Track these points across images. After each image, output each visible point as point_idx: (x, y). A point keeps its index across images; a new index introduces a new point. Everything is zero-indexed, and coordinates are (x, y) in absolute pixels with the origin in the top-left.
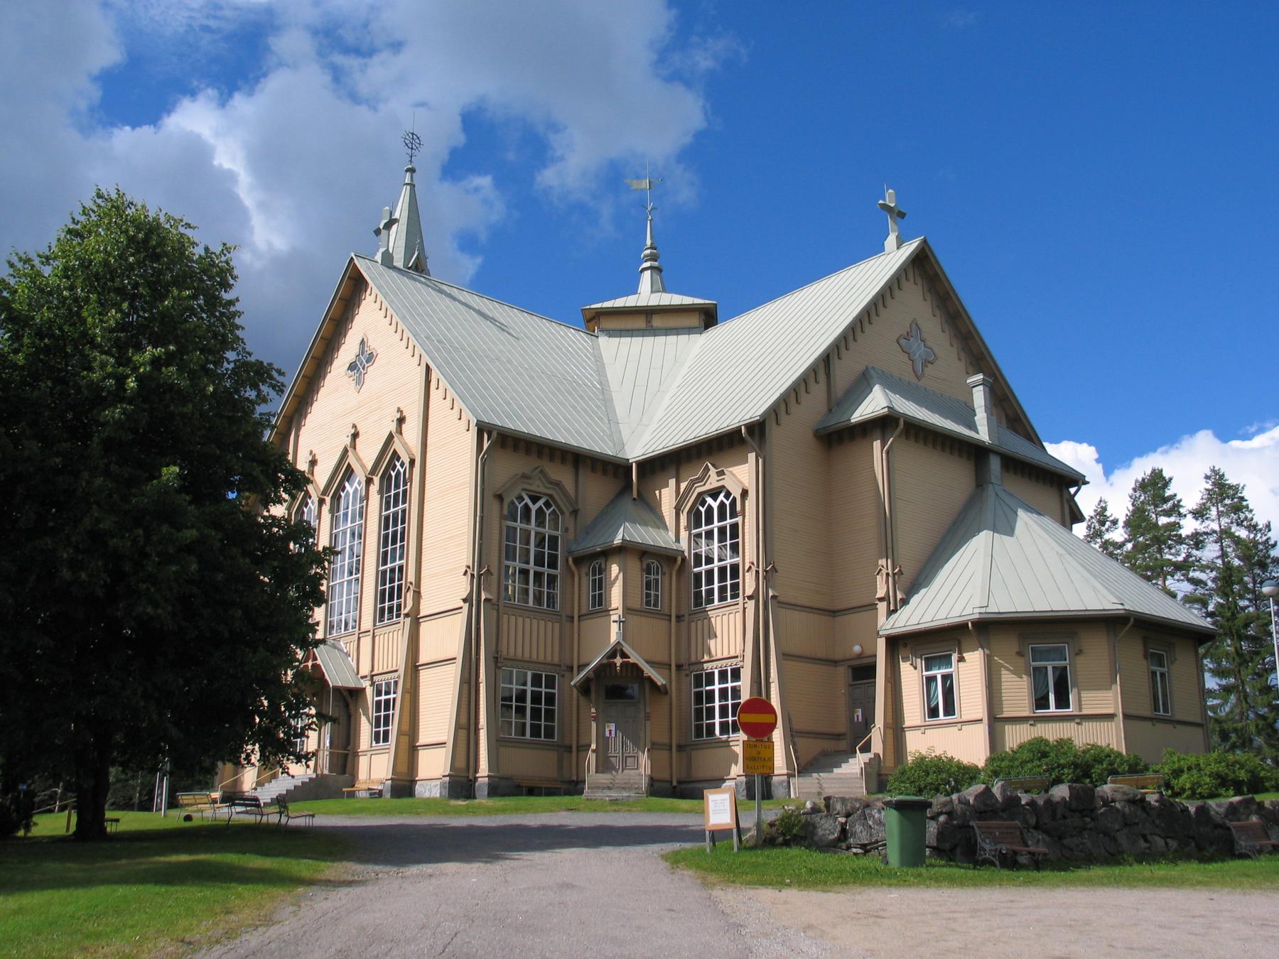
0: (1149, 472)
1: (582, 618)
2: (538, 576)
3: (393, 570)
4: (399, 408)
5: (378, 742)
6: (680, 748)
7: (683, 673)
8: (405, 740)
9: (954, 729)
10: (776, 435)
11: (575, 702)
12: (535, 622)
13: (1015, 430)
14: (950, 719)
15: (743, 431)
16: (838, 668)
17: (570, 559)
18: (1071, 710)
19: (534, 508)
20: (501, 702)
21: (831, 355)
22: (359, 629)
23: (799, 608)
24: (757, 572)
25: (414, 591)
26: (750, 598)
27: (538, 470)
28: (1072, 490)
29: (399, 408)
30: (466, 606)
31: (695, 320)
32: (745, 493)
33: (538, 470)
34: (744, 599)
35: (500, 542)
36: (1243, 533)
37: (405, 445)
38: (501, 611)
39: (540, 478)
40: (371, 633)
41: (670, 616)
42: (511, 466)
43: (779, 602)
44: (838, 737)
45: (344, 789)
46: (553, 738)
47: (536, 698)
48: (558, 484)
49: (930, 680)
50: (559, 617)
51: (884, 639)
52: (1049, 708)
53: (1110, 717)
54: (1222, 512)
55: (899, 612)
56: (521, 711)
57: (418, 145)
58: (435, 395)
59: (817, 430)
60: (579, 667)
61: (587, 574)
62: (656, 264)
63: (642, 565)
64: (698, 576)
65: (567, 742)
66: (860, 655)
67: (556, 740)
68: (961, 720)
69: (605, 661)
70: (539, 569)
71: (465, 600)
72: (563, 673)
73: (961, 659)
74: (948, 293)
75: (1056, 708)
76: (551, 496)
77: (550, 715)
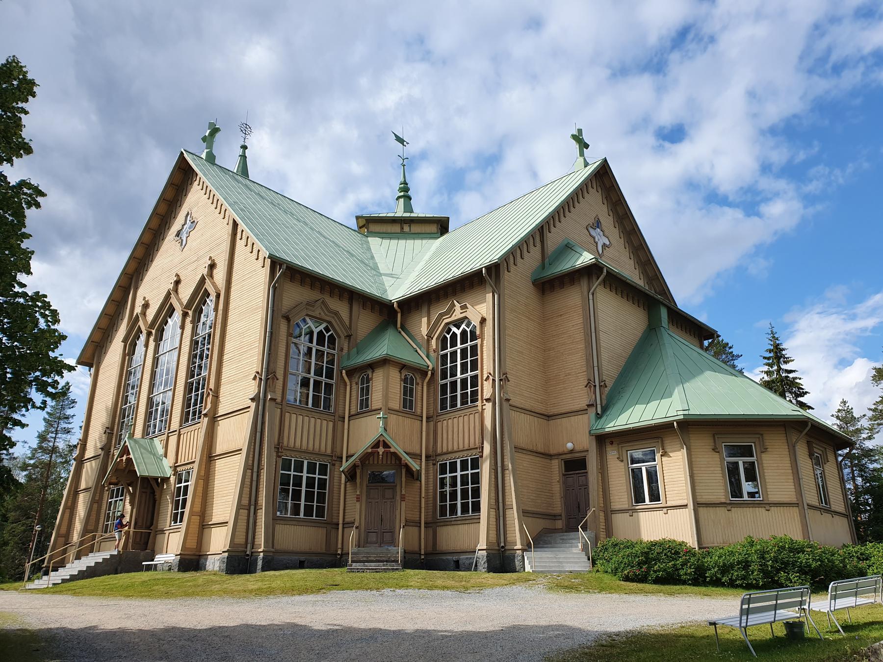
1: (352, 418)
2: (317, 384)
7: (431, 462)
8: (196, 519)
9: (660, 513)
10: (507, 277)
11: (343, 486)
14: (655, 504)
15: (484, 272)
16: (553, 461)
17: (344, 372)
22: (169, 430)
24: (494, 380)
25: (213, 396)
26: (488, 400)
30: (253, 405)
31: (434, 228)
32: (483, 321)
37: (214, 284)
41: (422, 417)
44: (554, 517)
45: (143, 563)
47: (310, 483)
48: (336, 314)
50: (333, 418)
53: (686, 506)
56: (297, 495)
60: (347, 457)
63: (401, 376)
65: (335, 521)
66: (571, 450)
67: (325, 519)
68: (667, 505)
71: (252, 400)
72: (334, 462)
73: (665, 454)
77: (321, 498)
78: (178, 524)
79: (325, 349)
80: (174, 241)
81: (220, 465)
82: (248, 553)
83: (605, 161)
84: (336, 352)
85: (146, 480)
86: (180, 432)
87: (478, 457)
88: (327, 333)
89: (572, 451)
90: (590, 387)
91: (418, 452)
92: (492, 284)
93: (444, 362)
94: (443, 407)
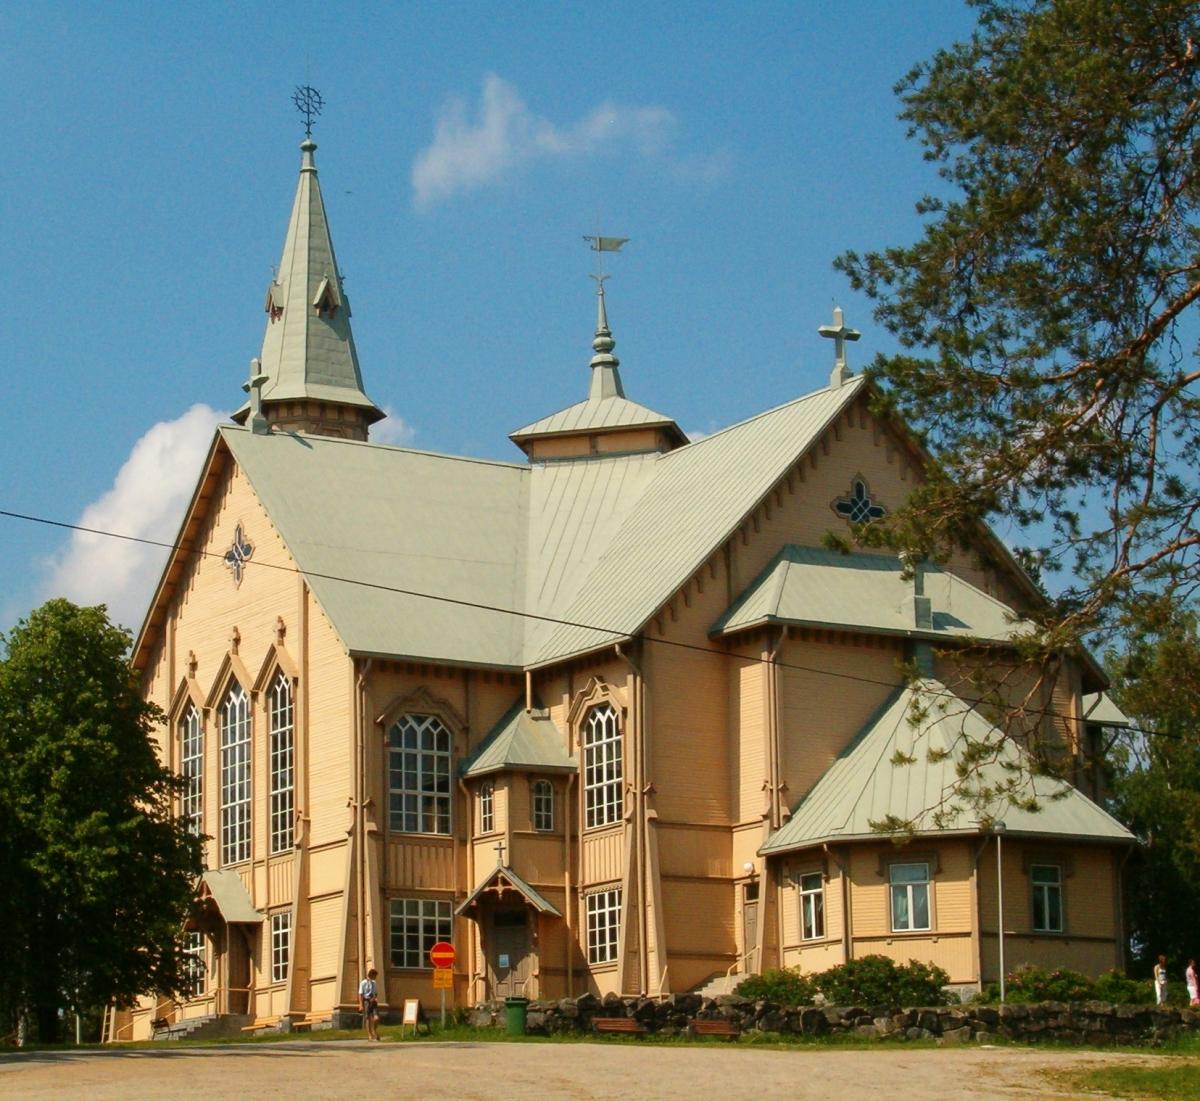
3: (283, 795)
4: (280, 618)
5: (278, 978)
9: (821, 950)
17: (461, 781)
19: (420, 730)
20: (391, 933)
29: (280, 618)
30: (351, 839)
32: (625, 711)
40: (265, 863)
42: (391, 688)
45: (243, 1029)
47: (429, 928)
49: (807, 899)
51: (764, 858)
52: (907, 927)
53: (968, 935)
55: (781, 829)
57: (317, 105)
58: (315, 610)
62: (608, 357)
69: (487, 889)
71: (349, 833)
75: (915, 927)
76: (438, 716)
78: (288, 849)
80: (223, 568)
81: (316, 909)
85: (237, 927)
86: (268, 863)
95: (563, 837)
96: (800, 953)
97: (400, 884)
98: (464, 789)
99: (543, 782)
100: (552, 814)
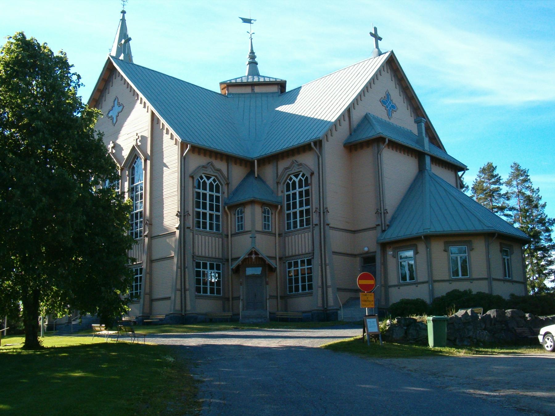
0: (486, 164)
6: (282, 297)
11: (230, 277)
12: (207, 238)
13: (433, 144)
17: (226, 207)
18: (468, 277)
19: (208, 182)
21: (351, 108)
23: (339, 230)
27: (211, 163)
28: (460, 174)
33: (211, 163)
34: (313, 226)
35: (193, 200)
36: (528, 193)
38: (194, 233)
39: (211, 168)
43: (330, 227)
46: (220, 294)
48: (219, 171)
54: (519, 183)
59: (345, 144)
61: (235, 214)
64: (289, 215)
70: (211, 212)
72: (224, 263)
74: (403, 78)
79: (215, 194)
82: (183, 314)
83: (392, 52)
84: (220, 194)
87: (311, 259)
88: (215, 183)
89: (367, 253)
90: (378, 214)
91: (274, 256)
92: (317, 152)
93: (288, 199)
94: (289, 228)
95: (275, 234)
96: (399, 288)
97: (200, 254)
98: (228, 211)
99: (267, 209)
100: (270, 223)
